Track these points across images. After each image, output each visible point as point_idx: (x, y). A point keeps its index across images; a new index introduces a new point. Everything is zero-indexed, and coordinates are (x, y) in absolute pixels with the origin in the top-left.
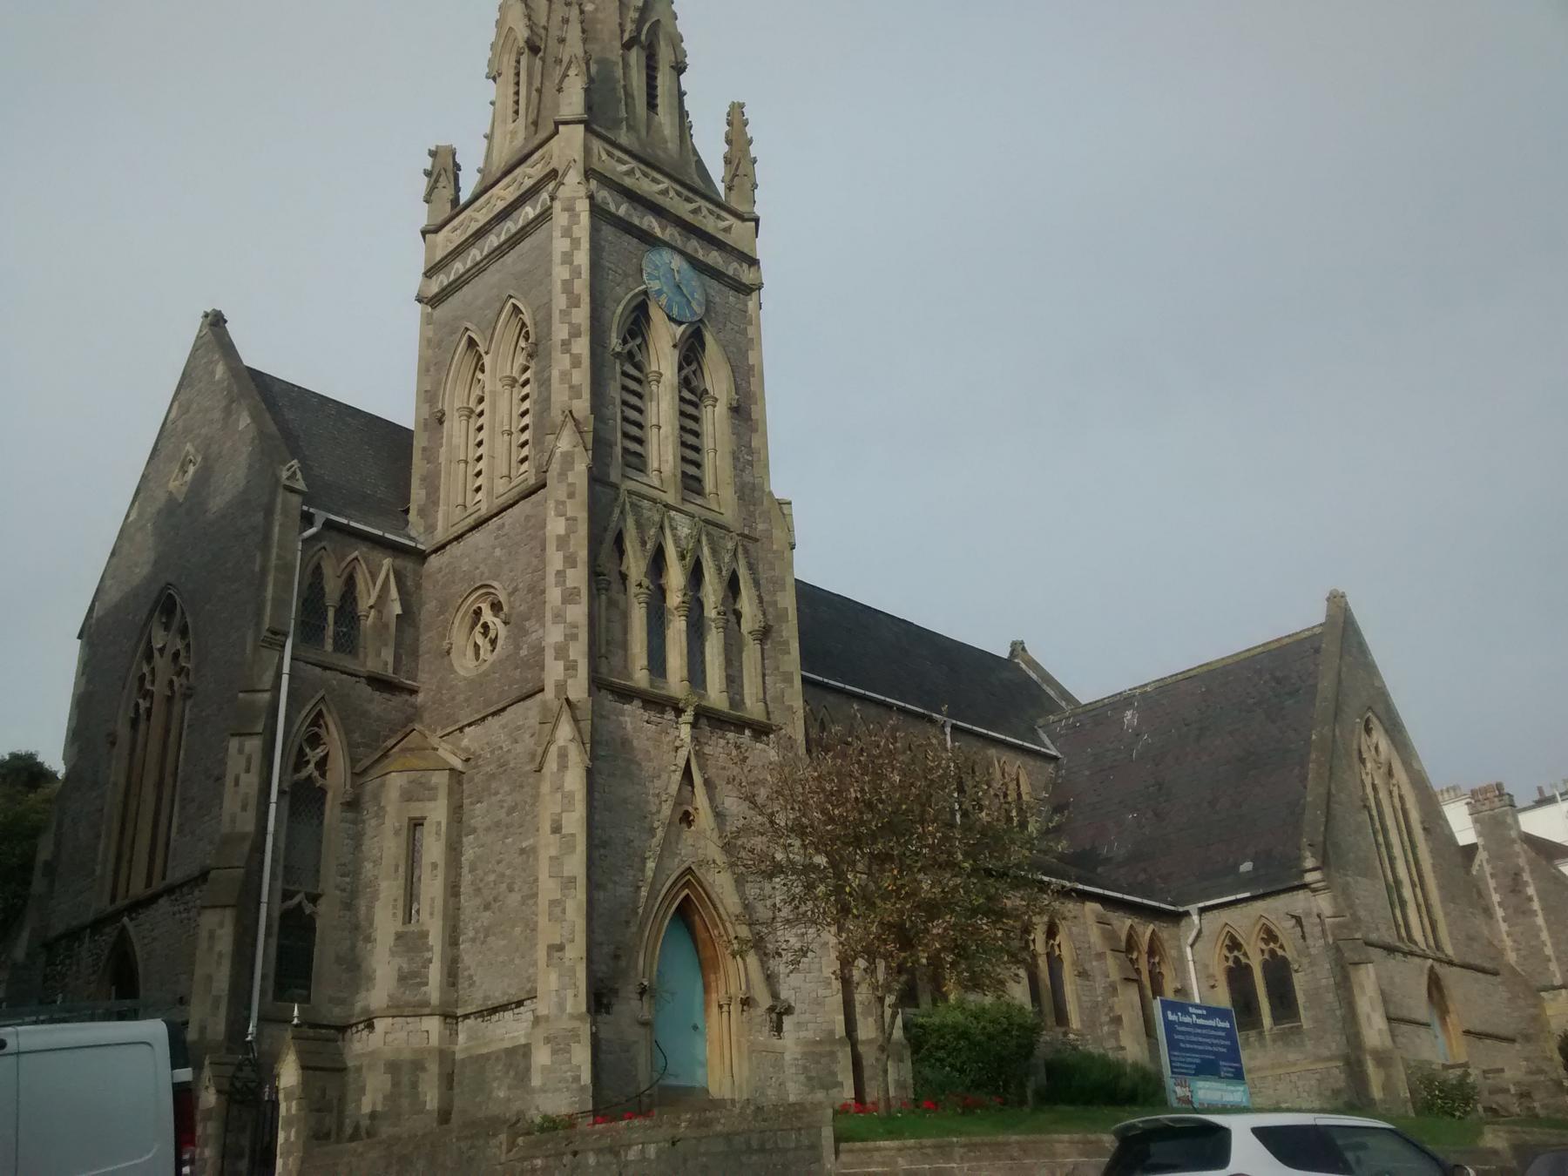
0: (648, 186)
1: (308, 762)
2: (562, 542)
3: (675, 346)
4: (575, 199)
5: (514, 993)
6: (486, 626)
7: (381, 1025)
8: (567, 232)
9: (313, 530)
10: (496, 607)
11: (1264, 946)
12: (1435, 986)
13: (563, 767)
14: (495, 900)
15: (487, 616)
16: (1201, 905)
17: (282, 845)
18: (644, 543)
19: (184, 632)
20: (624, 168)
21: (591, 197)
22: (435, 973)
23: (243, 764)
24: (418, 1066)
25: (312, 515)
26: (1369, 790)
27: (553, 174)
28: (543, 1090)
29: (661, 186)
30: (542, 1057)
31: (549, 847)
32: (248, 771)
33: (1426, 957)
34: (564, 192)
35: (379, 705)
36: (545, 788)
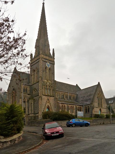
5: (37, 112)
7: (30, 115)
8: (40, 63)
10: (36, 89)
15: (35, 90)
18: (87, 125)
19: (15, 91)
22: (33, 112)
27: (40, 58)
30: (39, 116)
36: (39, 102)
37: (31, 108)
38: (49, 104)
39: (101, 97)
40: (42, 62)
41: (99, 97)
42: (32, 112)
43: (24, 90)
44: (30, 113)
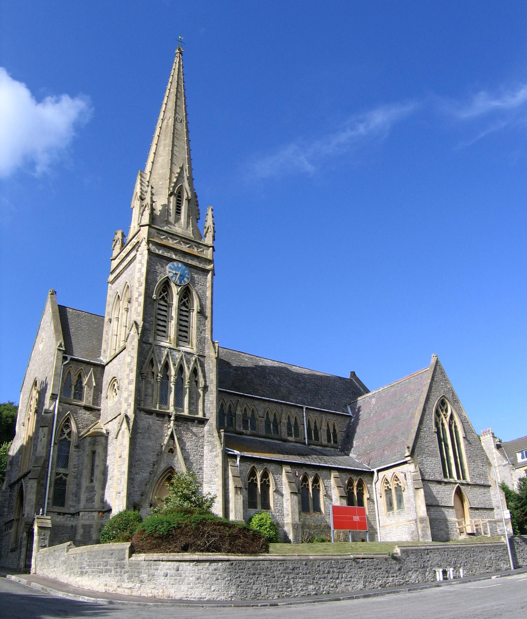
1: (65, 434)
3: (177, 294)
8: (141, 262)
9: (67, 362)
12: (459, 493)
13: (123, 437)
17: (55, 459)
33: (456, 483)
35: (87, 415)
37: (92, 481)
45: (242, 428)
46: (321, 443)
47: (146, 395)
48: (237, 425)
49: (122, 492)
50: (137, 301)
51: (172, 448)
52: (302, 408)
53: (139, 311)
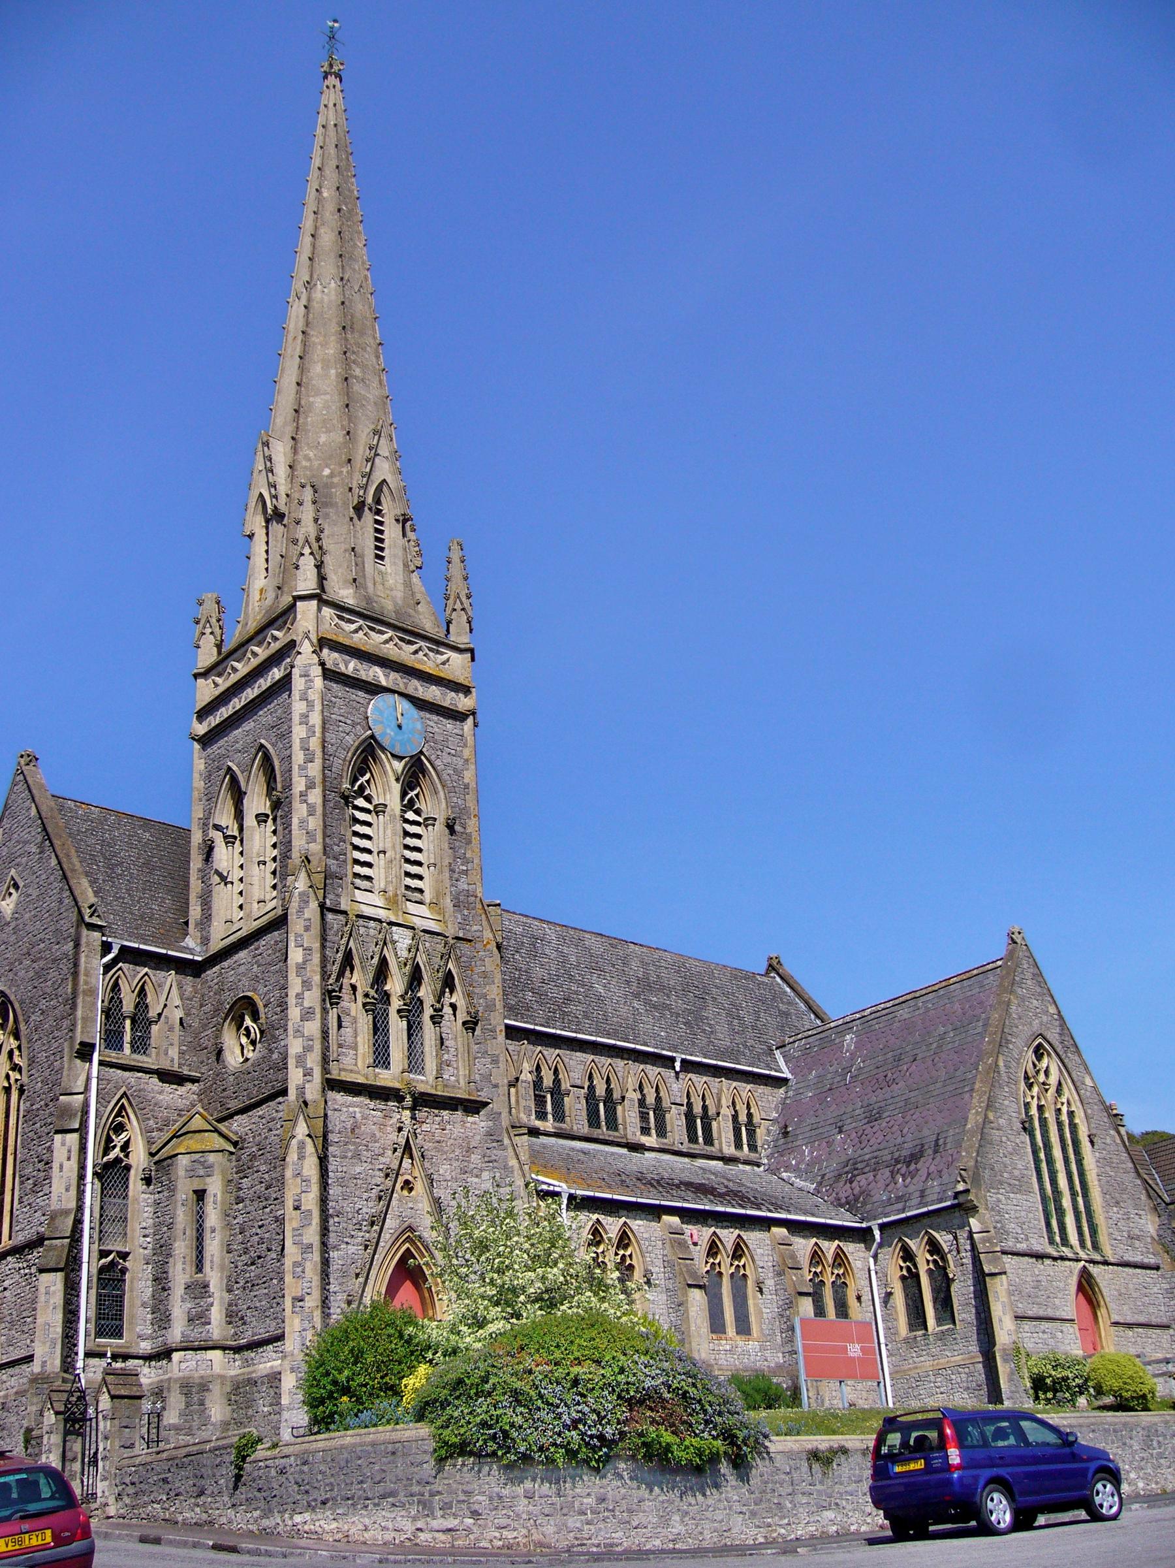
0: (377, 641)
1: (115, 1147)
2: (301, 967)
4: (310, 665)
6: (247, 1029)
7: (176, 1356)
8: (304, 697)
9: (111, 956)
11: (930, 1258)
12: (1087, 1287)
13: (301, 1157)
14: (259, 1257)
16: (880, 1221)
17: (97, 1215)
20: (353, 627)
21: (322, 664)
22: (217, 1314)
23: (66, 1155)
24: (204, 1387)
25: (110, 943)
26: (1034, 1111)
27: (292, 644)
28: (289, 1409)
29: (386, 636)
31: (292, 1221)
32: (69, 1159)
33: (1078, 1260)
34: (299, 661)
36: (289, 1173)
37: (199, 1268)
38: (425, 1205)
39: (1071, 1114)
40: (319, 682)
41: (1043, 1122)
42: (199, 1318)
43: (112, 1013)
44: (177, 1332)
45: (533, 1117)
46: (721, 1150)
47: (340, 1046)
48: (522, 1109)
49: (307, 1298)
50: (305, 801)
51: (410, 1178)
52: (673, 1059)
53: (311, 826)
